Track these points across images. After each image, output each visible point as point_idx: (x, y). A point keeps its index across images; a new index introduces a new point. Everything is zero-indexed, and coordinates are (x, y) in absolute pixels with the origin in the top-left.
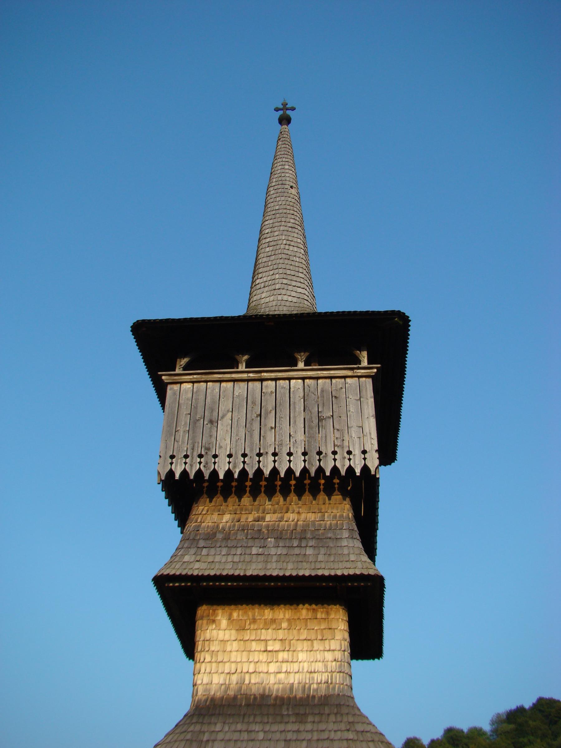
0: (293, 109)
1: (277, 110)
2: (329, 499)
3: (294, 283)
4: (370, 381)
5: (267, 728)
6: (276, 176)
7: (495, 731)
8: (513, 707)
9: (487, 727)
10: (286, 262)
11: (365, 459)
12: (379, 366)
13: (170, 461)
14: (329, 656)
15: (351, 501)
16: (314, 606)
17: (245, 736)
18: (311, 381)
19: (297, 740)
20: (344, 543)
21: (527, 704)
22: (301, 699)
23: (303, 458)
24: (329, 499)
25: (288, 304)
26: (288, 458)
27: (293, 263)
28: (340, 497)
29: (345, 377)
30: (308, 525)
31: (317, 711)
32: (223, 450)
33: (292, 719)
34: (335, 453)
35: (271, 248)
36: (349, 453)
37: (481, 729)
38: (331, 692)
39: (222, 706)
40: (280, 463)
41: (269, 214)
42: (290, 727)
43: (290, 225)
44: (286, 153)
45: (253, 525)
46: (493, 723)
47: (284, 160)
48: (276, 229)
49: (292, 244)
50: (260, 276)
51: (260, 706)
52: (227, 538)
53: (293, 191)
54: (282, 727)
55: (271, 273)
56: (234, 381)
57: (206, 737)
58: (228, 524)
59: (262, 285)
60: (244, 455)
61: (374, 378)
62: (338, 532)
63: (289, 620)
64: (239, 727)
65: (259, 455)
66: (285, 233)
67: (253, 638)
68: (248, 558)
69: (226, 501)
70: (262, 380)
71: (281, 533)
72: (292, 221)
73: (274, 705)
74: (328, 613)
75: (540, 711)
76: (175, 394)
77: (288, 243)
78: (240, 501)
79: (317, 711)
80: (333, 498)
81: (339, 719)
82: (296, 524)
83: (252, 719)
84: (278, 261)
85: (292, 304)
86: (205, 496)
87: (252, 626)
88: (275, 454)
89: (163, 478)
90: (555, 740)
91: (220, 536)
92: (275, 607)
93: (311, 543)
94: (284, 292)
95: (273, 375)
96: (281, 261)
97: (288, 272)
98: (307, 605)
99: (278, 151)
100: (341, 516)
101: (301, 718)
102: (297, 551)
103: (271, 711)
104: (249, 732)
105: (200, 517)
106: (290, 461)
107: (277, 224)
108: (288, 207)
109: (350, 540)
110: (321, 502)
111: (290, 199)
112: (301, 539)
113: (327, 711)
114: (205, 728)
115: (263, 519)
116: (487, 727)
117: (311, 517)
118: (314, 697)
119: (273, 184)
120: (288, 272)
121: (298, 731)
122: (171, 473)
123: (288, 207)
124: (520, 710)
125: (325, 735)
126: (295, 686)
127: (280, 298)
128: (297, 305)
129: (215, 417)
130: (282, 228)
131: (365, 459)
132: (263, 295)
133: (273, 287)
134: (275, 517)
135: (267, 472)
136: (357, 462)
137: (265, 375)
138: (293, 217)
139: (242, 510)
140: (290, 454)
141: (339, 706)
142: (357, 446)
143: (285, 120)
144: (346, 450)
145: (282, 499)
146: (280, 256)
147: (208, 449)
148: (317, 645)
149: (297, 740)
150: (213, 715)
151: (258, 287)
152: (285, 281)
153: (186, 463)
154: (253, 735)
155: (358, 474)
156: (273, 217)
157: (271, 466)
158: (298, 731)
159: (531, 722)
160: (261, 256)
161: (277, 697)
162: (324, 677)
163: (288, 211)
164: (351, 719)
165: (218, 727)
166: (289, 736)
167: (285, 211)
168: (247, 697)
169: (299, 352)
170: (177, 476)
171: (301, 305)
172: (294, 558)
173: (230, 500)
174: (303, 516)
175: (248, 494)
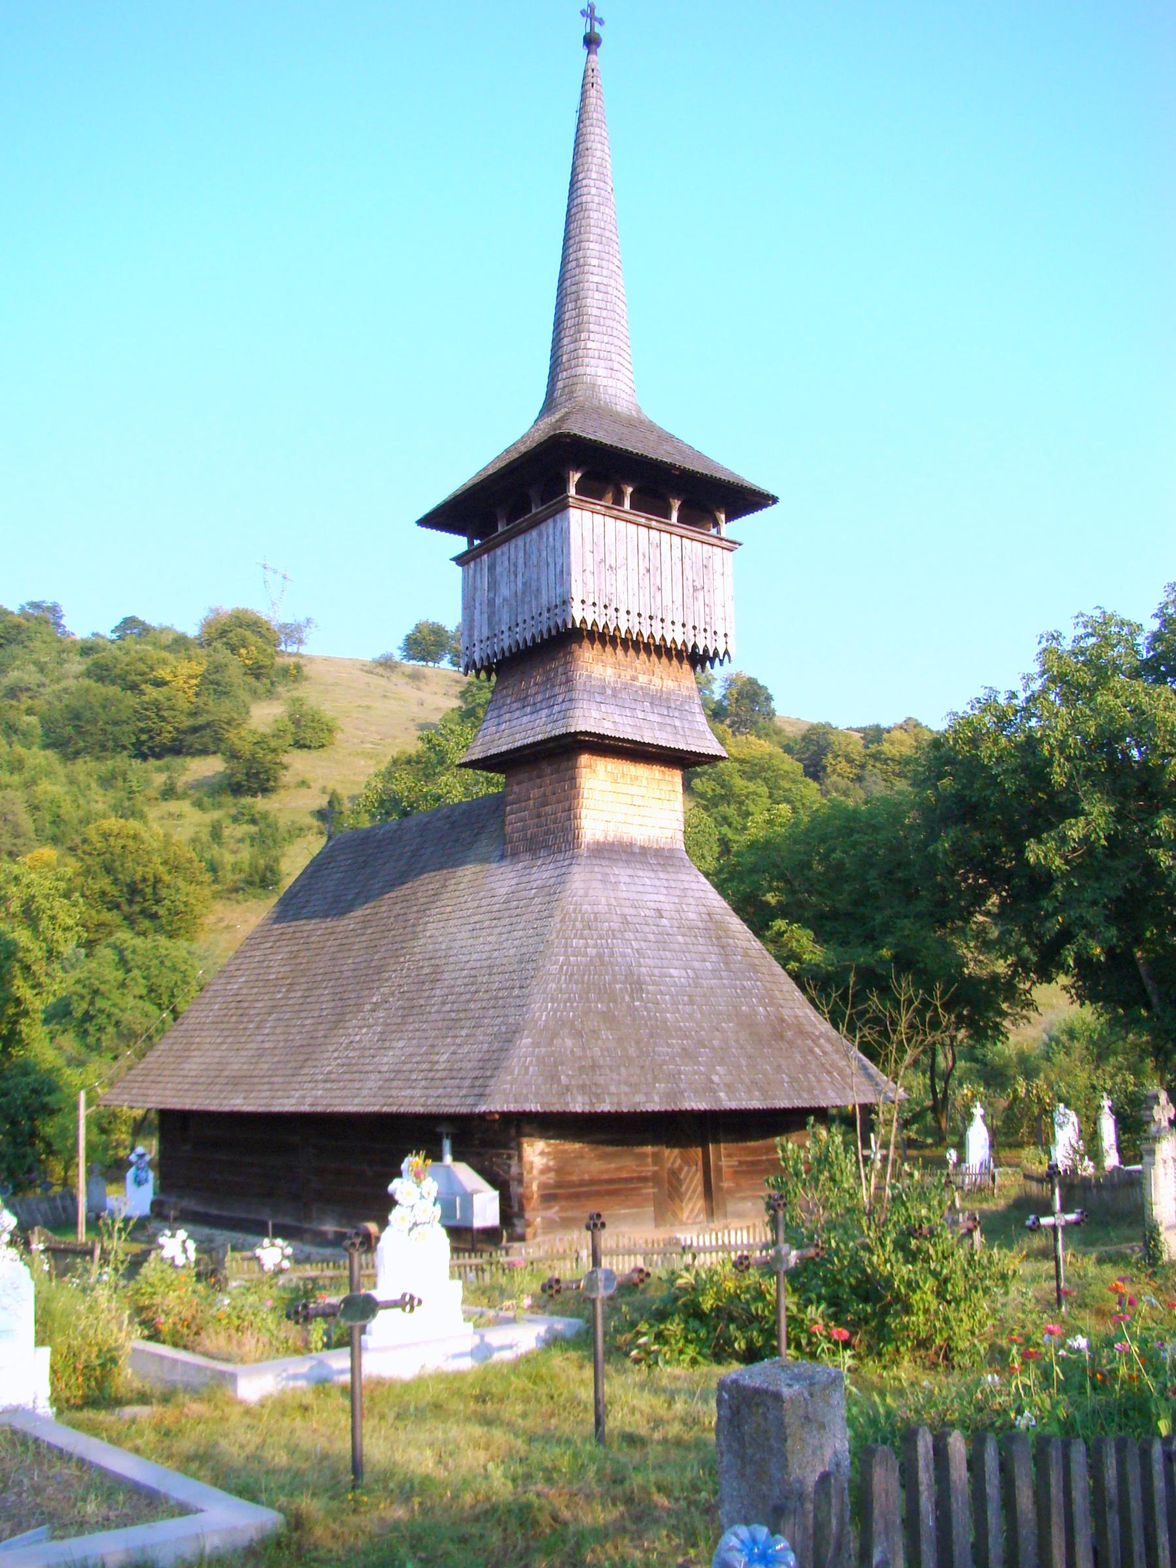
34: (705, 630)
36: (715, 633)
55: (606, 339)
58: (612, 679)
91: (609, 692)
137: (654, 524)
147: (611, 600)
168: (621, 844)
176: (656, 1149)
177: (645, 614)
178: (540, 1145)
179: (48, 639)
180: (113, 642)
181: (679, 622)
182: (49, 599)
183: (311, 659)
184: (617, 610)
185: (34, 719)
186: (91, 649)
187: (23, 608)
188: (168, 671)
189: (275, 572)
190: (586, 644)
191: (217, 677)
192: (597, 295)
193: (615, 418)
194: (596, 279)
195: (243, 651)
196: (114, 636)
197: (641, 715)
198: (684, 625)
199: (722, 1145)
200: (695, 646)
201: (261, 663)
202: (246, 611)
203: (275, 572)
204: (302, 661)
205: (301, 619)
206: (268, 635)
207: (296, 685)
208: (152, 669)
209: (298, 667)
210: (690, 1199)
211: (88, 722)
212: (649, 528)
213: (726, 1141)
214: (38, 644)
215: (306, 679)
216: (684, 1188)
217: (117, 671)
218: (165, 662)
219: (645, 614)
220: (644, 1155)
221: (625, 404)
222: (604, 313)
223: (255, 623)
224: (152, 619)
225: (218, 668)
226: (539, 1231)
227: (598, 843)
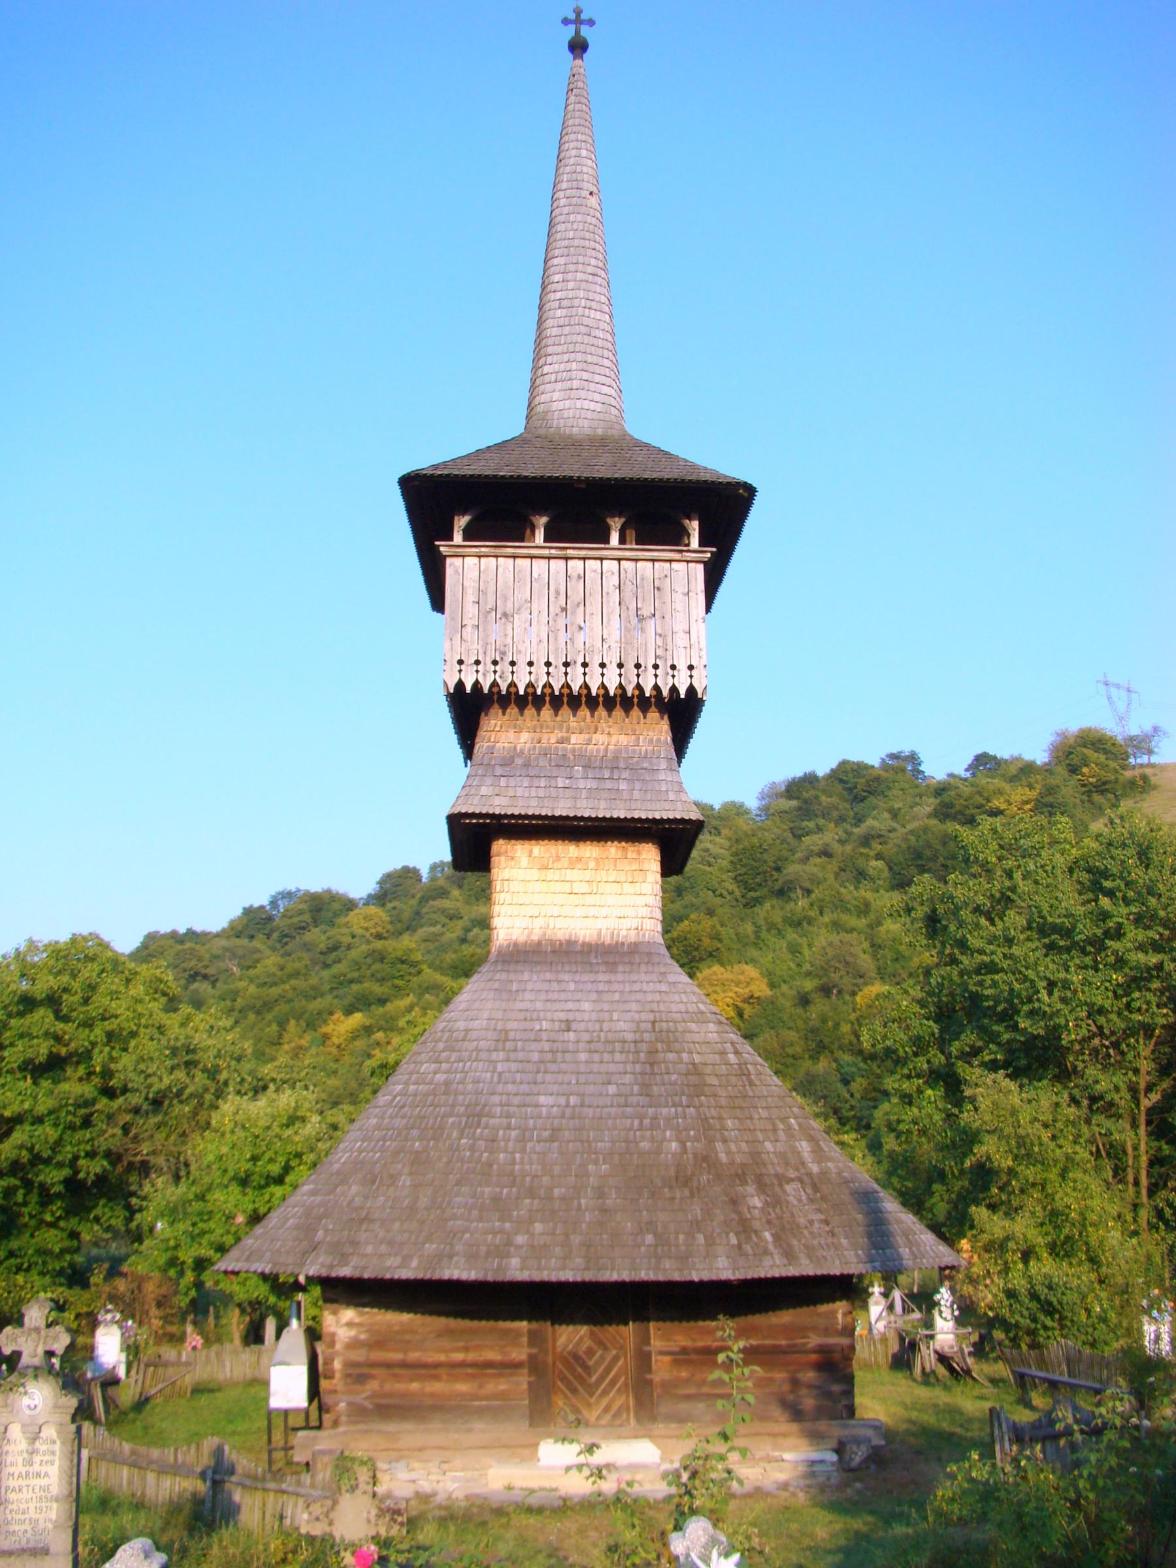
0: (591, 23)
1: (566, 22)
2: (645, 717)
3: (597, 378)
4: (701, 567)
5: (577, 977)
6: (568, 169)
7: (765, 809)
8: (799, 773)
9: (752, 803)
10: (587, 339)
11: (691, 677)
12: (714, 549)
13: (458, 667)
14: (642, 900)
15: (669, 718)
16: (623, 844)
17: (555, 986)
18: (629, 563)
19: (609, 991)
20: (662, 776)
21: (822, 770)
22: (610, 945)
23: (618, 671)
24: (645, 717)
25: (589, 415)
26: (600, 670)
27: (595, 341)
28: (657, 714)
29: (670, 561)
30: (620, 751)
31: (627, 960)
32: (522, 656)
33: (603, 968)
34: (656, 667)
35: (564, 312)
36: (673, 667)
37: (742, 805)
38: (641, 939)
39: (527, 952)
40: (591, 677)
41: (559, 244)
42: (601, 977)
43: (590, 270)
44: (582, 122)
45: (557, 748)
46: (762, 797)
47: (580, 137)
48: (570, 276)
49: (594, 305)
50: (549, 359)
51: (567, 953)
52: (527, 765)
53: (593, 201)
54: (592, 977)
55: (566, 357)
56: (532, 557)
57: (515, 987)
58: (528, 745)
59: (553, 377)
60: (548, 664)
61: (705, 564)
62: (655, 761)
63: (596, 859)
64: (548, 976)
65: (566, 664)
66: (584, 285)
67: (557, 878)
68: (553, 792)
69: (522, 714)
70: (567, 559)
71: (589, 759)
72: (593, 262)
73: (581, 952)
74: (639, 853)
75: (841, 781)
76: (457, 572)
77: (588, 304)
78: (539, 715)
79: (627, 960)
80: (649, 715)
81: (651, 969)
82: (606, 749)
84: (574, 338)
85: (595, 415)
86: (496, 706)
87: (556, 865)
88: (585, 665)
89: (452, 691)
90: (856, 825)
92: (581, 844)
93: (625, 775)
94: (583, 394)
95: (583, 553)
96: (579, 338)
97: (590, 358)
98: (616, 843)
99: (569, 116)
100: (659, 740)
101: (612, 967)
102: (609, 784)
103: (579, 959)
104: (559, 982)
105: (493, 734)
106: (603, 675)
107: (572, 268)
108: (587, 235)
109: (669, 773)
110: (635, 721)
111: (589, 219)
112: (613, 768)
113: (637, 959)
114: (512, 976)
115: (568, 740)
116: (752, 803)
117: (624, 740)
118: (623, 944)
119: (564, 185)
120: (590, 358)
121: (610, 982)
122: (460, 685)
123: (587, 235)
124: (810, 780)
125: (637, 987)
126: (603, 932)
127: (579, 404)
128: (602, 416)
129: (509, 610)
130: (579, 276)
131: (691, 677)
132: (556, 396)
133: (568, 384)
134: (582, 738)
135: (576, 688)
136: (682, 680)
137: (570, 552)
138: (594, 253)
139: (542, 726)
140: (603, 665)
141: (649, 954)
143: (578, 47)
144: (669, 663)
145: (588, 713)
146: (577, 329)
147: (503, 653)
148: (628, 888)
149: (609, 991)
150: (517, 962)
151: (547, 379)
152: (585, 375)
153: (477, 671)
154: (563, 986)
155: (682, 696)
156: (566, 251)
157: (580, 681)
158: (610, 982)
159: (823, 798)
160: (549, 323)
161: (584, 944)
162: (634, 923)
163: (587, 243)
164: (663, 970)
165: (526, 976)
166: (601, 987)
167: (583, 243)
168: (552, 942)
169: (613, 516)
171: (607, 417)
172: (605, 795)
173: (526, 712)
174: (614, 739)
175: (547, 705)
176: (535, 1325)
177: (557, 661)
178: (349, 1314)
179: (906, 786)
180: (965, 780)
181: (612, 660)
182: (906, 748)
183: (1163, 768)
184: (513, 663)
185: (880, 864)
186: (943, 790)
187: (883, 760)
188: (1002, 800)
189: (1118, 686)
190: (496, 710)
191: (1050, 799)
192: (559, 313)
193: (575, 444)
194: (559, 295)
195: (1085, 770)
196: (968, 775)
197: (561, 783)
198: (620, 666)
199: (652, 1324)
200: (674, 689)
201: (1104, 779)
202: (1090, 730)
203: (1118, 686)
204: (1148, 771)
205: (1148, 728)
206: (1113, 750)
207: (1145, 795)
208: (988, 801)
209: (1144, 778)
210: (605, 1392)
211: (929, 859)
213: (658, 1319)
214: (895, 792)
215: (1155, 788)
216: (594, 1379)
217: (958, 808)
218: (1000, 792)
219: (557, 661)
220: (517, 1334)
221: (586, 423)
222: (567, 330)
223: (1100, 741)
224: (1002, 750)
225: (1050, 790)
226: (343, 1419)
227: (515, 944)
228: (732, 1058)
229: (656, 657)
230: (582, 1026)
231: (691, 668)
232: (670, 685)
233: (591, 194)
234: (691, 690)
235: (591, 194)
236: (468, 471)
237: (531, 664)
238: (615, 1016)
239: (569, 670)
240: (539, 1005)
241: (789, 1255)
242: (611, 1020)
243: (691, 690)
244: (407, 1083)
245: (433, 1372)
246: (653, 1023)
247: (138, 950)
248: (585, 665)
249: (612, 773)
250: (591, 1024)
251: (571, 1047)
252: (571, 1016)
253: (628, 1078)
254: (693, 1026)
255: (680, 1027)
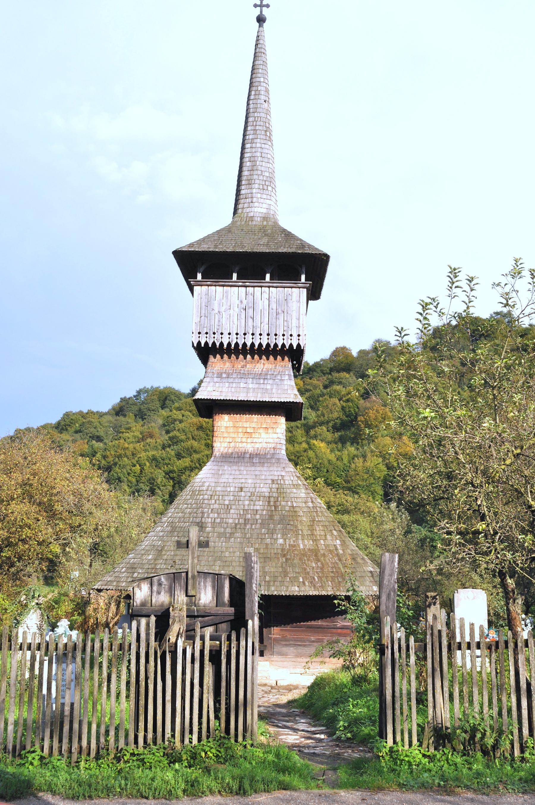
0: (268, 6)
33: (258, 465)
34: (284, 335)
36: (291, 335)
54: (253, 468)
60: (237, 334)
83: (240, 464)
88: (253, 334)
101: (262, 464)
102: (262, 386)
109: (289, 381)
122: (199, 343)
140: (261, 335)
142: (295, 332)
143: (261, 20)
144: (290, 334)
153: (206, 337)
154: (241, 472)
155: (295, 348)
170: (203, 345)
184: (222, 334)
197: (242, 385)
200: (291, 345)
212: (246, 287)
228: (310, 504)
229: (284, 331)
230: (248, 490)
231: (299, 336)
232: (290, 343)
233: (265, 101)
234: (299, 345)
235: (265, 101)
236: (204, 248)
237: (229, 334)
238: (262, 486)
239: (246, 336)
240: (230, 481)
241: (268, 591)
242: (260, 487)
243: (299, 345)
244: (173, 513)
245: (466, 699)
246: (278, 489)
247: (59, 423)
248: (253, 334)
249: (264, 381)
250: (251, 489)
251: (242, 498)
252: (243, 485)
253: (264, 512)
254: (295, 490)
255: (288, 491)
